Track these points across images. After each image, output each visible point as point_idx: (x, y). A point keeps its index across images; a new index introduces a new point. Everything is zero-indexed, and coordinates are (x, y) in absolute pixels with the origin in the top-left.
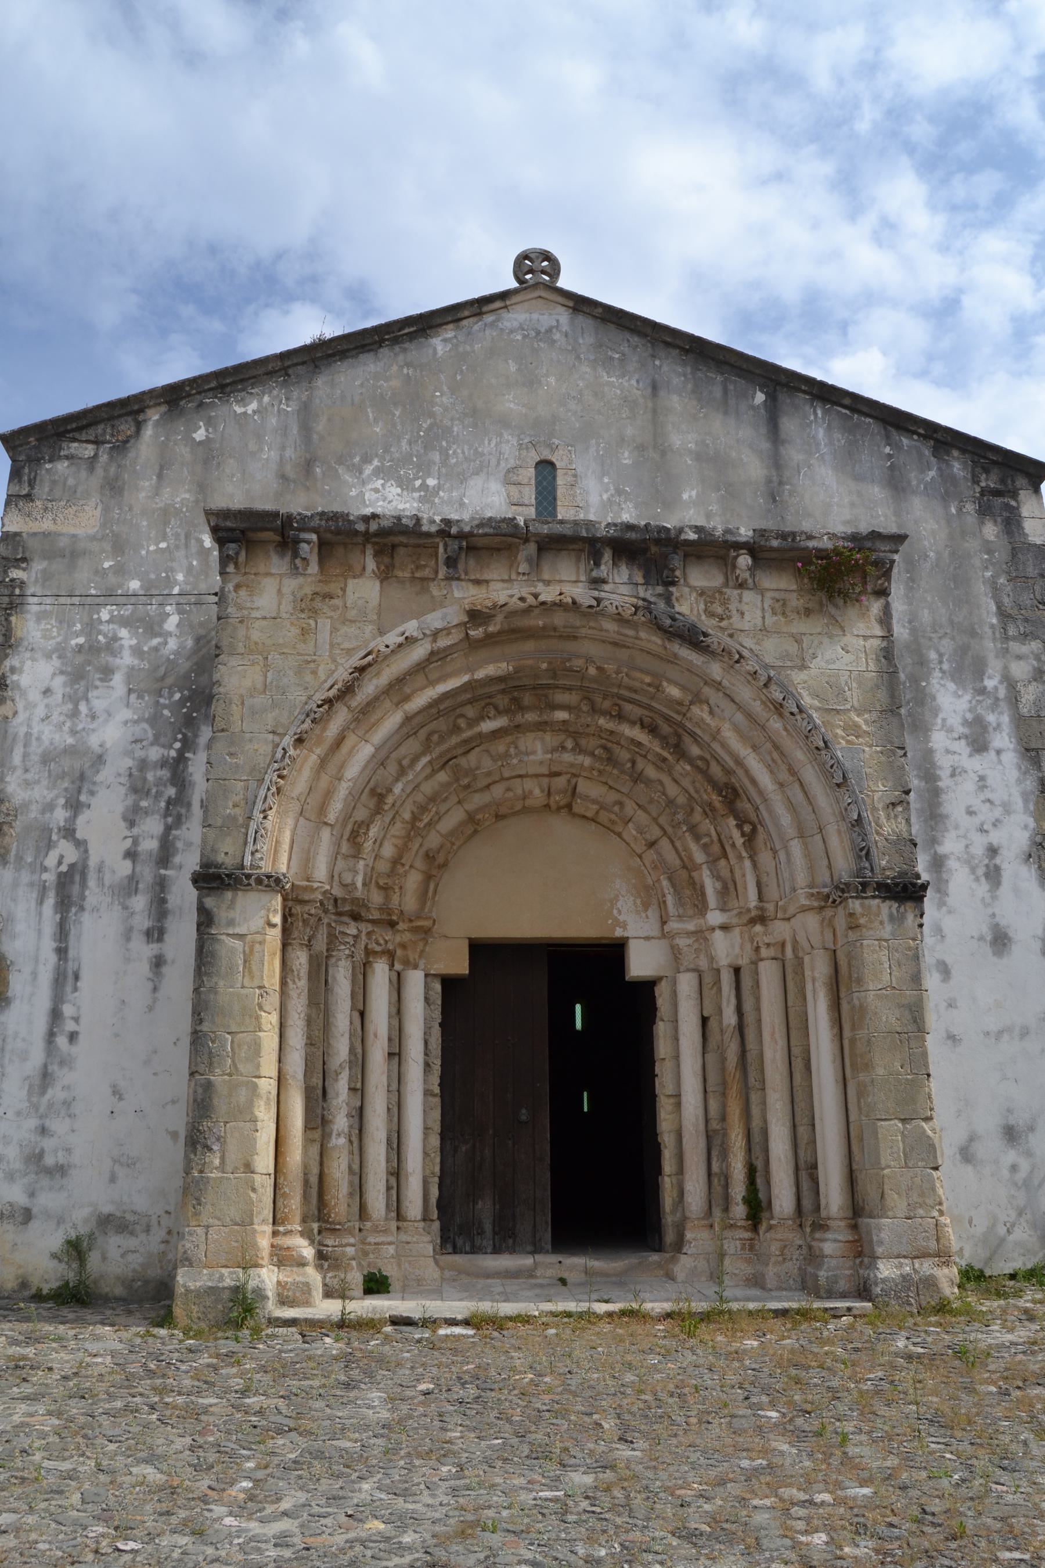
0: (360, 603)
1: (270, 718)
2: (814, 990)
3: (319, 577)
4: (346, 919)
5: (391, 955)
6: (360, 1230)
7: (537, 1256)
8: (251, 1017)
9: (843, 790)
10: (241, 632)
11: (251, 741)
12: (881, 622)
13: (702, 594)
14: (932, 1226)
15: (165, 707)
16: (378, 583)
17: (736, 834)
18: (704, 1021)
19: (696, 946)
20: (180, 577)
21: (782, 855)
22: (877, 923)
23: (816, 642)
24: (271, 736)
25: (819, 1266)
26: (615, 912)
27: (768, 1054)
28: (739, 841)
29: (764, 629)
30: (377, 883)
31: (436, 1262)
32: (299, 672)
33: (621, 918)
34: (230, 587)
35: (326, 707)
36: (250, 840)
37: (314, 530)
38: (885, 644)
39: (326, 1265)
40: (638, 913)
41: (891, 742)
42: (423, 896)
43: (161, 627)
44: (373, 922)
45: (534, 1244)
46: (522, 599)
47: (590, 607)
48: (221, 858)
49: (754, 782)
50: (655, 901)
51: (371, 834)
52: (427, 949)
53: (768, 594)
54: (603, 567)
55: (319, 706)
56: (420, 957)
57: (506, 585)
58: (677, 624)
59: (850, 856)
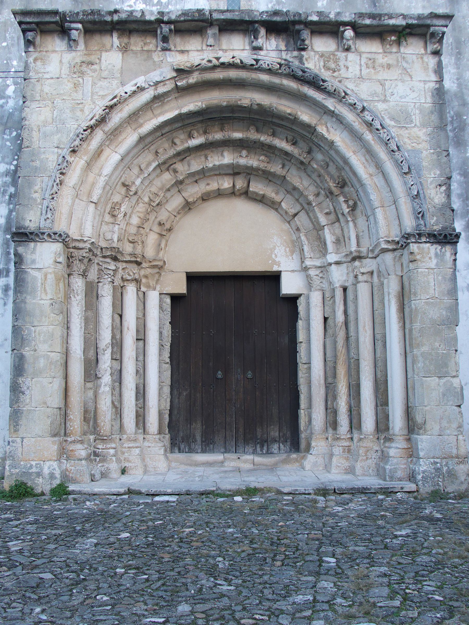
0: (110, 67)
1: (56, 139)
2: (389, 300)
3: (85, 52)
4: (108, 260)
5: (137, 281)
6: (120, 439)
7: (225, 455)
8: (46, 317)
9: (408, 176)
10: (38, 88)
11: (44, 153)
12: (435, 72)
13: (322, 56)
14: (455, 440)
15: (8, 140)
16: (120, 55)
17: (344, 206)
18: (326, 319)
19: (321, 275)
20: (15, 63)
21: (371, 218)
22: (427, 259)
23: (393, 85)
24: (56, 150)
25: (386, 463)
26: (273, 256)
27: (361, 339)
28: (346, 210)
29: (361, 77)
30: (128, 240)
31: (167, 458)
32: (73, 110)
33: (277, 260)
34: (31, 60)
35: (89, 131)
36: (44, 212)
37: (80, 22)
38: (437, 86)
39: (98, 459)
40: (287, 256)
41: (440, 147)
42: (159, 248)
43: (4, 93)
44: (126, 262)
45: (226, 449)
46: (210, 61)
47: (252, 65)
48: (27, 223)
49: (355, 174)
50: (298, 250)
51: (122, 209)
52: (161, 279)
53: (364, 56)
54: (260, 40)
55: (84, 131)
56: (157, 283)
57: (199, 53)
58: (306, 75)
59: (412, 217)
